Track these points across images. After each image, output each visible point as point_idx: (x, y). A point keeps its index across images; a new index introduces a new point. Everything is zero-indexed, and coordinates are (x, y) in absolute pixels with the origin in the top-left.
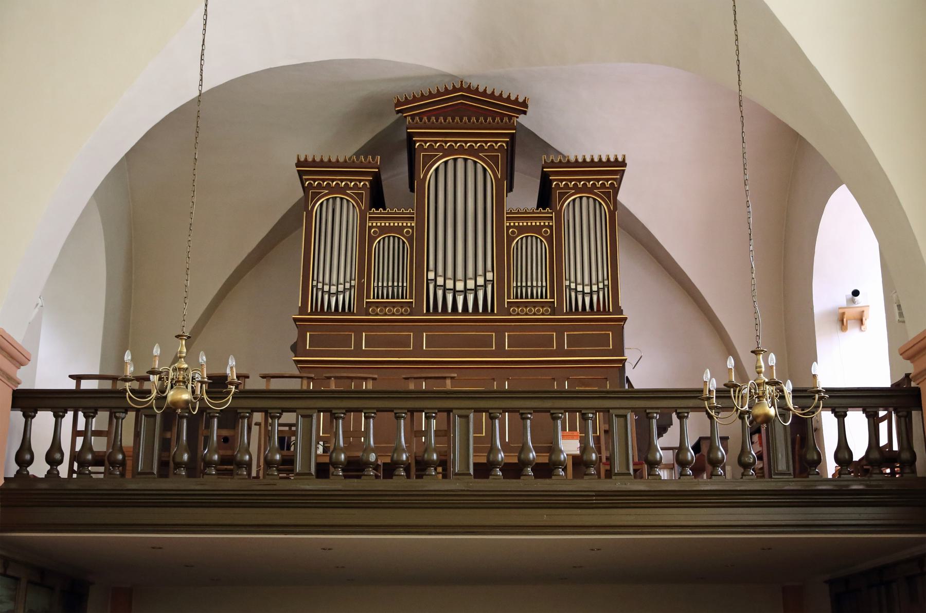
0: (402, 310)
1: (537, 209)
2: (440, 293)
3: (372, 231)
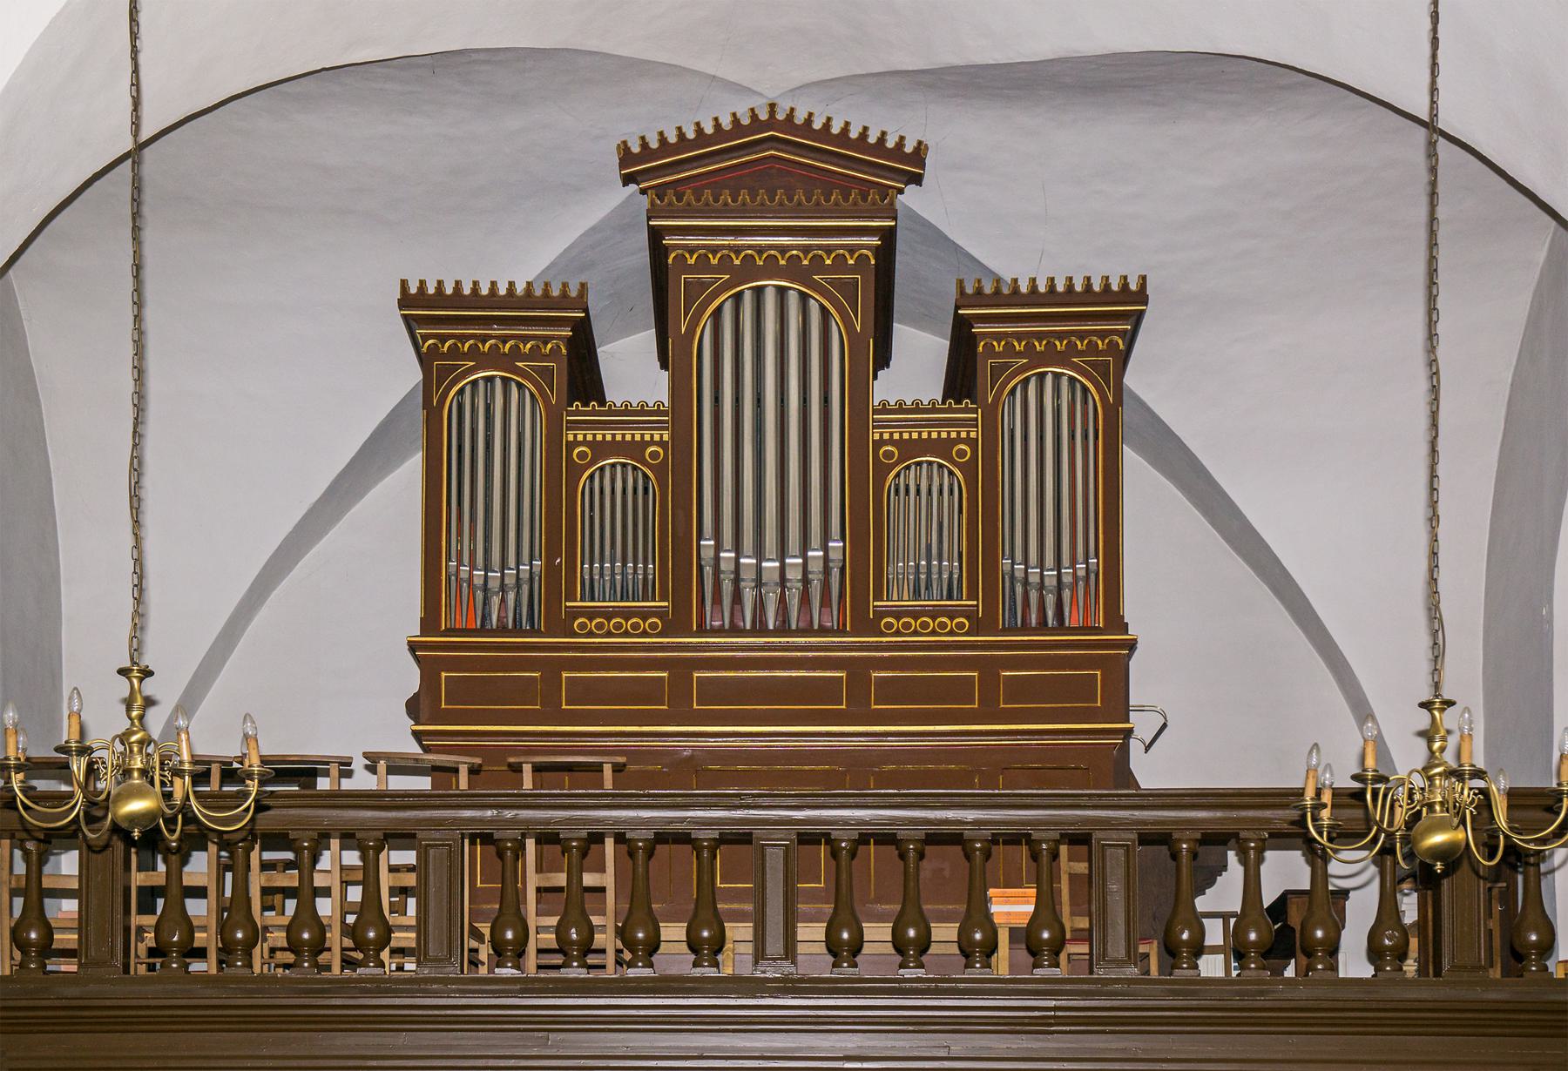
0: (644, 625)
1: (944, 402)
3: (576, 451)
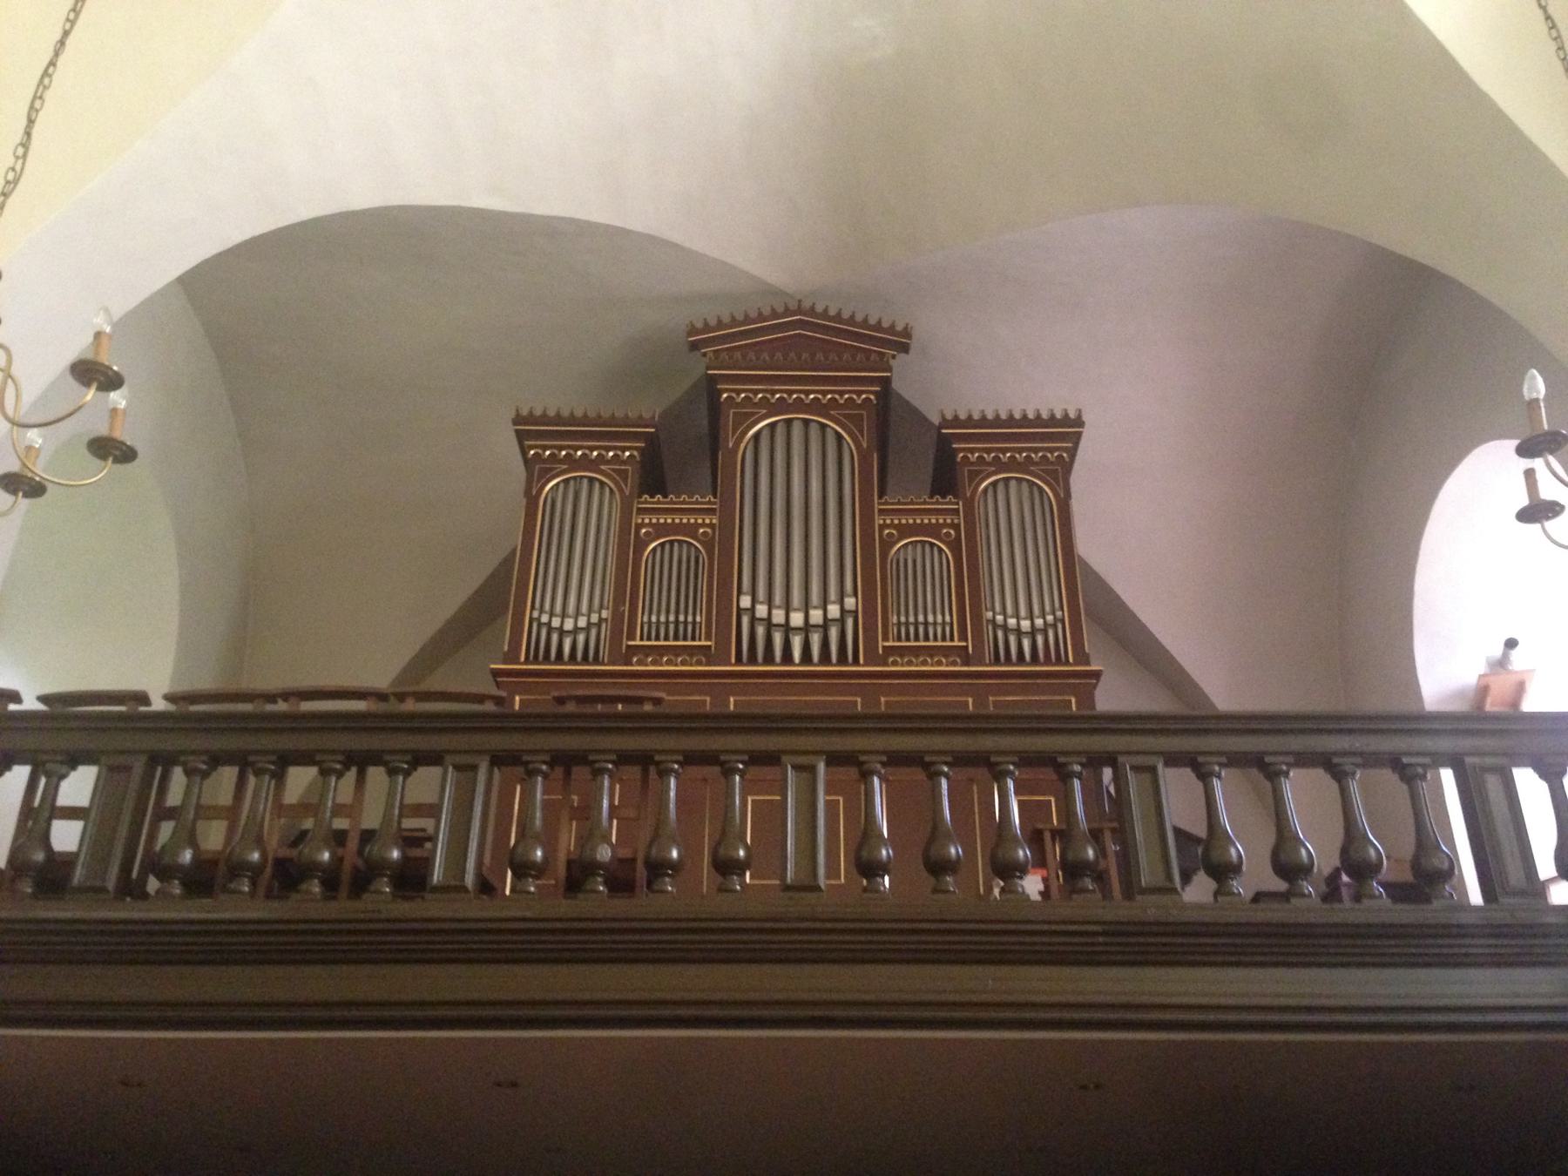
2: (760, 630)
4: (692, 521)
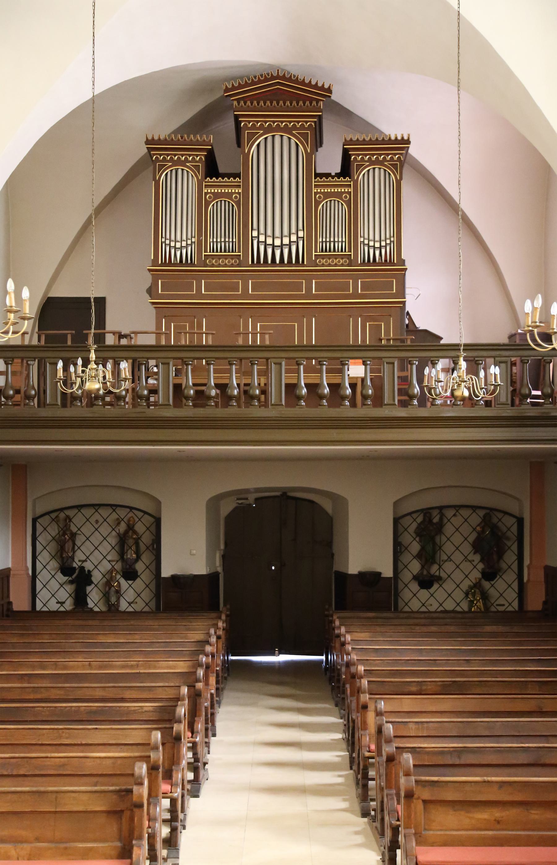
4: (230, 191)
